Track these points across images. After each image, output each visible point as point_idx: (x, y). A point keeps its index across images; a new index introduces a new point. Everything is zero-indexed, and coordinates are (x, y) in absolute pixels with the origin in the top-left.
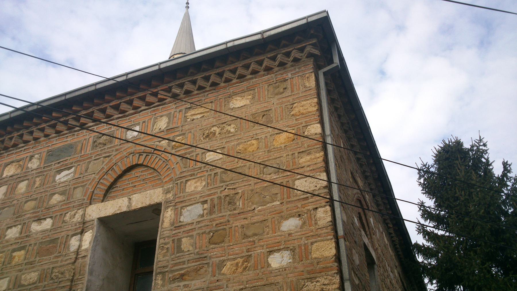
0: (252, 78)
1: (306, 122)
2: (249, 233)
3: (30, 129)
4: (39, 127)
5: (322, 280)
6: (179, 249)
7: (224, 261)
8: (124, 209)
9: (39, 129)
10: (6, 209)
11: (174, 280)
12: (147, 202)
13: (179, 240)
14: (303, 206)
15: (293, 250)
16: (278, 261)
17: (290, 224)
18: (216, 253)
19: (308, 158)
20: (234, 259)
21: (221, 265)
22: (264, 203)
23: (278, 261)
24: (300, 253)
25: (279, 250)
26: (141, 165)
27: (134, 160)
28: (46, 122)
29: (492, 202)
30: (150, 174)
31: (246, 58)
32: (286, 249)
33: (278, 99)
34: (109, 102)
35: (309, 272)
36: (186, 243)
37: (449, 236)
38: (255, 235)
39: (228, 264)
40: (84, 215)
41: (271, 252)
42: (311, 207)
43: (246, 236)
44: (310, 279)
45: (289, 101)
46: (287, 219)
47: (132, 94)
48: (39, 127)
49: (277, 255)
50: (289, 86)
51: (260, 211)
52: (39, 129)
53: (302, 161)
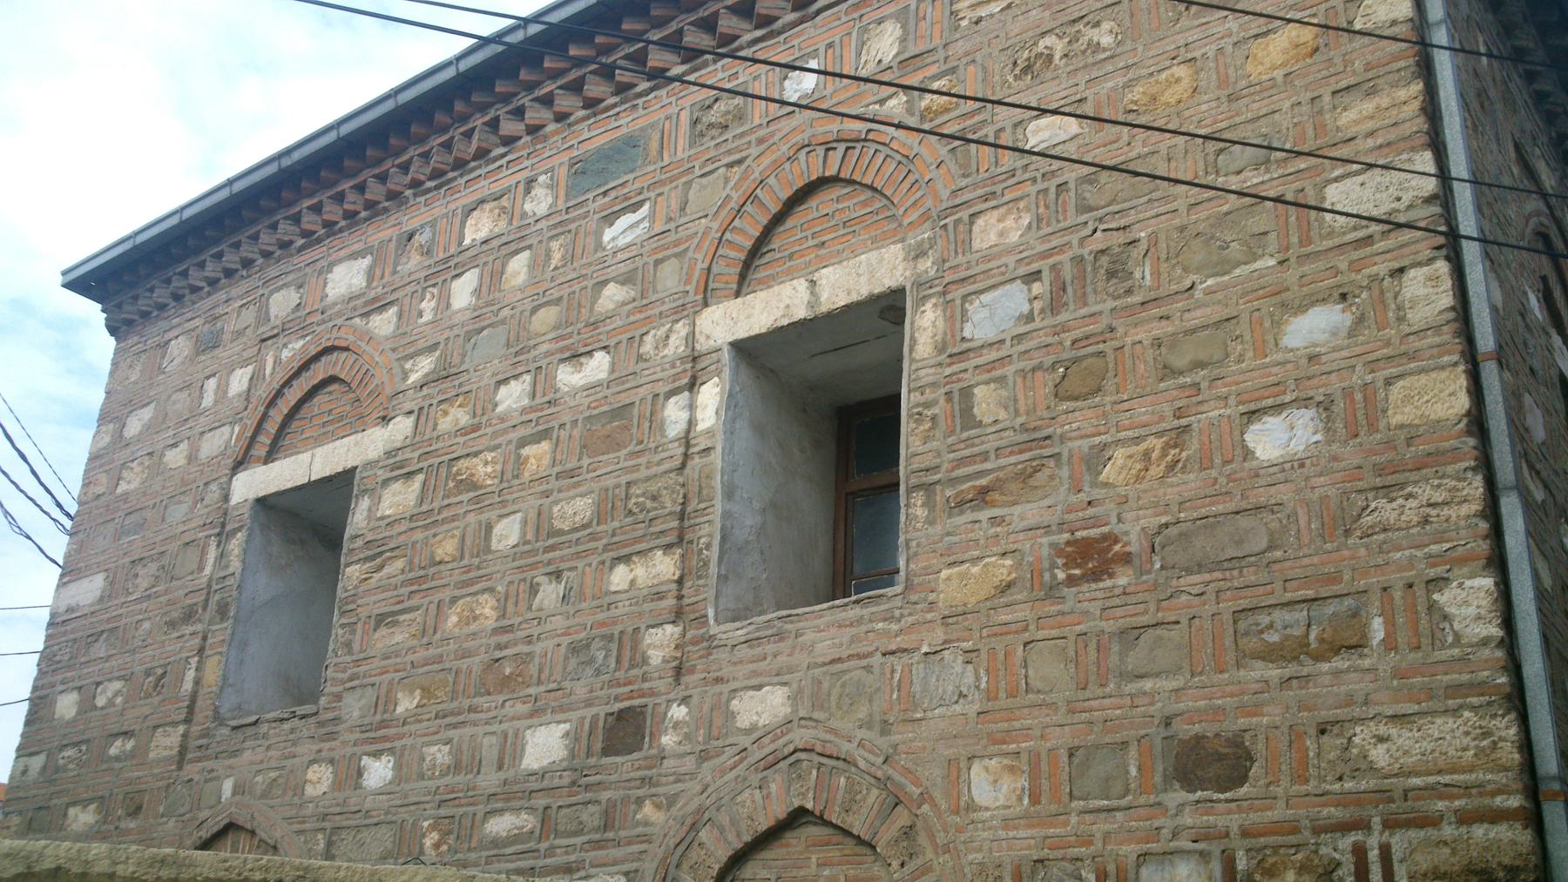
2: (1179, 362)
5: (1426, 492)
6: (967, 417)
8: (801, 313)
11: (961, 504)
12: (862, 288)
13: (966, 393)
14: (1355, 266)
15: (1326, 406)
17: (1316, 326)
18: (1078, 425)
19: (1368, 106)
20: (1137, 440)
21: (1097, 458)
22: (1224, 267)
23: (1272, 440)
24: (1350, 412)
25: (1278, 408)
26: (835, 180)
28: (555, 75)
30: (864, 204)
32: (1305, 402)
35: (1380, 470)
36: (986, 402)
38: (1199, 365)
39: (1120, 454)
40: (691, 338)
41: (1252, 415)
42: (1381, 269)
43: (1168, 371)
44: (1386, 490)
46: (1302, 309)
49: (1272, 422)
53: (1350, 115)
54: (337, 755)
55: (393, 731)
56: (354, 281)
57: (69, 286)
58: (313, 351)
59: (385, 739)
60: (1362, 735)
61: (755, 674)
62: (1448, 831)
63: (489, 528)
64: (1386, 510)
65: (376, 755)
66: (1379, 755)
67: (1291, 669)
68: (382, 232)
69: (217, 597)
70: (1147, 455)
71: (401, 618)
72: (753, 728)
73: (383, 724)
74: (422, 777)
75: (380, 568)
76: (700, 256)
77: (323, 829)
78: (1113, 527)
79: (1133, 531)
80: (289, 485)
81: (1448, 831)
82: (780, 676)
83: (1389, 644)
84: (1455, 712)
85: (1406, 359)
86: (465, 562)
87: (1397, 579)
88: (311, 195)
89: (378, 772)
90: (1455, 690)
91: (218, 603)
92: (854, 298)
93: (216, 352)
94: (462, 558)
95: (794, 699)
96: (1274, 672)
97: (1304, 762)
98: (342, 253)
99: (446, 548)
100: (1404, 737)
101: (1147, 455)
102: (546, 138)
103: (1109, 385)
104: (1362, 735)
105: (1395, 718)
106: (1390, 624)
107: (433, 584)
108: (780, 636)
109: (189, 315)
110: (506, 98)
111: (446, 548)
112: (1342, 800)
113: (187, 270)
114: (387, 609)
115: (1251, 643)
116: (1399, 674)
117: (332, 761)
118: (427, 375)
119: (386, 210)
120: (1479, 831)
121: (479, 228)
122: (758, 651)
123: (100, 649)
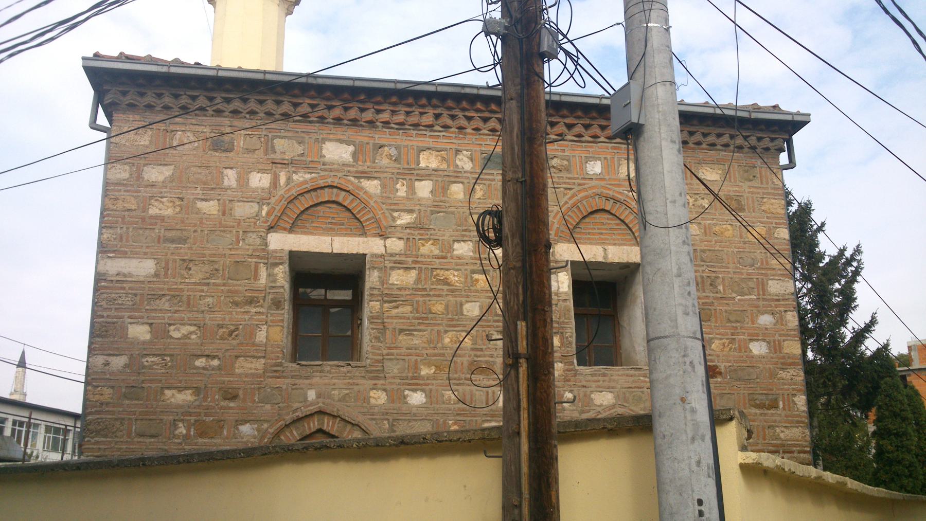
0: (722, 150)
1: (776, 223)
2: (732, 319)
3: (453, 112)
4: (467, 114)
7: (712, 338)
8: (600, 259)
9: (465, 116)
10: (442, 214)
12: (624, 259)
14: (776, 306)
15: (769, 343)
16: (758, 349)
17: (766, 320)
20: (721, 339)
22: (742, 294)
24: (775, 347)
25: (758, 340)
26: (608, 212)
27: (600, 203)
28: (478, 111)
29: (887, 468)
30: (618, 225)
31: (723, 127)
32: (764, 340)
33: (750, 187)
34: (564, 117)
35: (783, 364)
37: (823, 460)
38: (737, 321)
42: (782, 309)
43: (729, 321)
44: (782, 369)
45: (759, 193)
46: (763, 314)
47: (593, 118)
48: (467, 114)
49: (756, 343)
50: (758, 176)
51: (739, 300)
52: (465, 116)
54: (388, 387)
55: (420, 382)
56: (344, 155)
57: (87, 70)
58: (321, 183)
59: (417, 384)
60: (778, 430)
61: (599, 387)
62: (795, 455)
63: (462, 305)
64: (782, 374)
65: (414, 391)
66: (782, 435)
67: (762, 411)
68: (363, 136)
69: (271, 296)
70: (724, 344)
71: (415, 333)
72: (601, 405)
73: (413, 378)
74: (444, 403)
75: (397, 307)
76: (377, 136)
77: (387, 419)
78: (718, 364)
79: (722, 366)
80: (317, 250)
81: (795, 455)
82: (609, 389)
83: (784, 408)
84: (797, 427)
85: (785, 366)
86: (450, 316)
87: (786, 393)
88: (312, 98)
89: (417, 398)
90: (798, 422)
91: (272, 299)
92: (621, 261)
93: (228, 154)
94: (448, 314)
95: (617, 397)
96: (758, 411)
97: (765, 435)
98: (331, 136)
99: (439, 308)
100: (787, 432)
101: (724, 344)
102: (465, 134)
103: (713, 319)
104: (778, 430)
105: (786, 427)
106: (784, 403)
107: (432, 322)
108: (604, 375)
109: (194, 121)
110: (450, 109)
111: (439, 308)
112: (774, 445)
113: (197, 97)
114: (405, 327)
115: (752, 403)
116: (786, 416)
117: (385, 390)
118: (409, 223)
119: (362, 126)
120: (802, 455)
121: (429, 161)
122: (596, 378)
123: (164, 304)
